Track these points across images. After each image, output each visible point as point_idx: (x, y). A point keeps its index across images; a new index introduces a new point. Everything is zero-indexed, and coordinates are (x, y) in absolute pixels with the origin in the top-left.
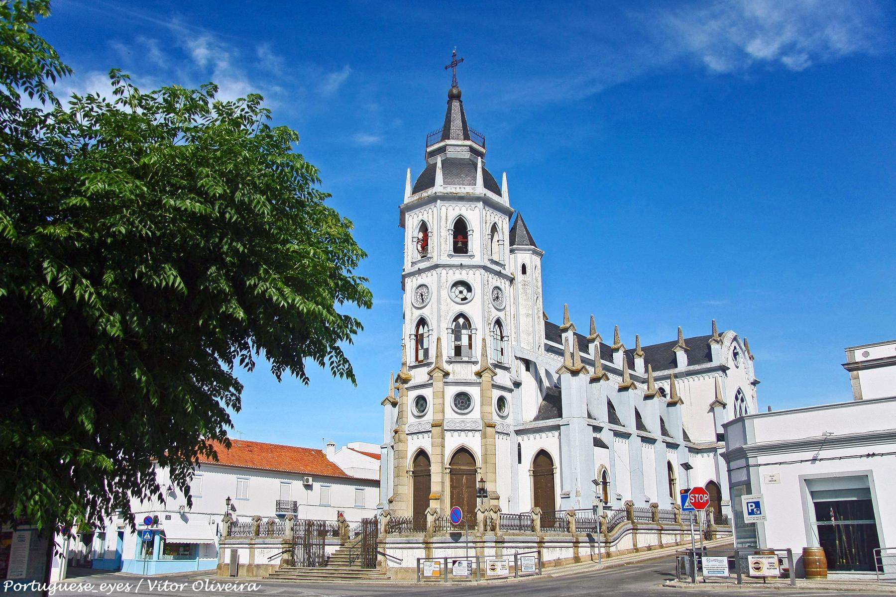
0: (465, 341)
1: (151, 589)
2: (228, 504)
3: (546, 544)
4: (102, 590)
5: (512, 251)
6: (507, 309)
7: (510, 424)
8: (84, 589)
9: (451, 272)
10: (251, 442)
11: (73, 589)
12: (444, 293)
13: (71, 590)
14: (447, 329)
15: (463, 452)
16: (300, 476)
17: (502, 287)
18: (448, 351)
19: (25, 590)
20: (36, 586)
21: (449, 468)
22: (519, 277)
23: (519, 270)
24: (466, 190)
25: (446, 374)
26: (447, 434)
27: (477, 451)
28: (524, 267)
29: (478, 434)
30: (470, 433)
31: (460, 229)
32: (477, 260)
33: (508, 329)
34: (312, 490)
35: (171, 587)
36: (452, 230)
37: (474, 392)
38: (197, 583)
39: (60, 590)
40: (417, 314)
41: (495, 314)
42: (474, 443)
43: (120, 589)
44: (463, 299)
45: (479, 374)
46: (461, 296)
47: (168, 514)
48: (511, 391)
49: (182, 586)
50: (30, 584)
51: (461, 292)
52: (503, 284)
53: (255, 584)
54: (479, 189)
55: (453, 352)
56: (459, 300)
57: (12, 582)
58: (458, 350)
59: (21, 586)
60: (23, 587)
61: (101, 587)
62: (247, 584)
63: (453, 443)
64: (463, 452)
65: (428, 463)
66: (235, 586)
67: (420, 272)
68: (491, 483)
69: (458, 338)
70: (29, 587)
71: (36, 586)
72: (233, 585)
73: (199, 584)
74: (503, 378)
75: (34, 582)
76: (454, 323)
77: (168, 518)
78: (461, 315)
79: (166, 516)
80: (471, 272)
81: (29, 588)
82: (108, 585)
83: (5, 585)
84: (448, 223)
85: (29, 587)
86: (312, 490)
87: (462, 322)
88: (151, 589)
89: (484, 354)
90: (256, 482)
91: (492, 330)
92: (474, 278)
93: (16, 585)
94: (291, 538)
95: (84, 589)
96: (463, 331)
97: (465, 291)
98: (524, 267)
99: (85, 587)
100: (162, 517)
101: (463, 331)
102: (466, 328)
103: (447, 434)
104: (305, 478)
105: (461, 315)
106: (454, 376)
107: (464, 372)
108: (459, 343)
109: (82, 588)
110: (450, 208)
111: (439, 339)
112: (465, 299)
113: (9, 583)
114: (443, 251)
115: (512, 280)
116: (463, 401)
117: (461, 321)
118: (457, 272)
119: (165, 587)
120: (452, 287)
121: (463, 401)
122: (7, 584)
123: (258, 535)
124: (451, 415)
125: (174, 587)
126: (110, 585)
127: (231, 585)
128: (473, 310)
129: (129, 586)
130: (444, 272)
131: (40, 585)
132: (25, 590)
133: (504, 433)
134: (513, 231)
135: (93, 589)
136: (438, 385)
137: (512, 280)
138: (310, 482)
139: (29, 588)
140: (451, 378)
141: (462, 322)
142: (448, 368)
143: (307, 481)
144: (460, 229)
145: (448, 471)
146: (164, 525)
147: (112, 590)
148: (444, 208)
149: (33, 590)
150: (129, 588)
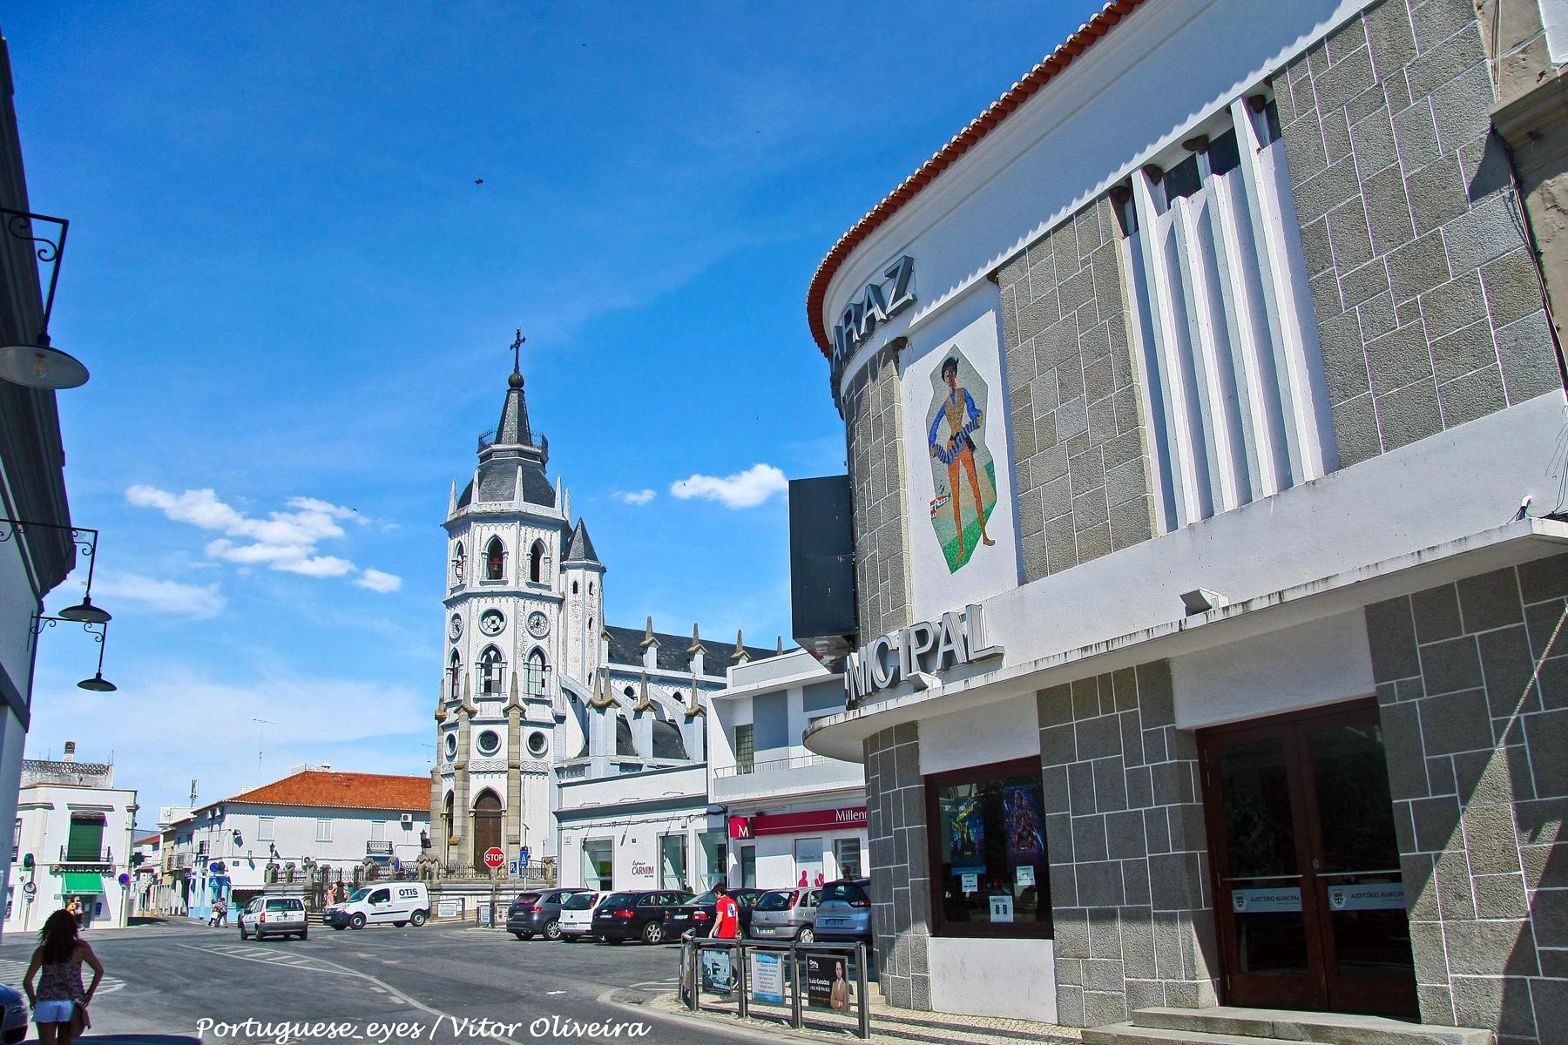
0: (495, 676)
1: (457, 1034)
2: (272, 851)
3: (503, 892)
4: (370, 1035)
5: (563, 569)
6: (553, 634)
7: (550, 760)
8: (338, 1032)
9: (482, 600)
10: (351, 774)
11: (318, 1033)
12: (475, 622)
13: (316, 1035)
14: (476, 664)
15: (488, 794)
16: (394, 814)
17: (547, 613)
18: (476, 688)
19: (234, 1034)
20: (254, 1028)
21: (473, 812)
22: (570, 596)
23: (569, 589)
24: (503, 506)
25: (472, 713)
26: (472, 777)
27: (502, 791)
28: (575, 585)
29: (505, 775)
30: (496, 776)
31: (496, 551)
32: (511, 587)
33: (551, 660)
34: (411, 829)
35: (493, 1028)
36: (485, 554)
37: (502, 731)
38: (538, 1022)
39: (297, 1034)
40: (488, 641)
41: (532, 643)
42: (499, 784)
43: (402, 1033)
44: (495, 630)
45: (506, 711)
46: (494, 626)
47: (237, 860)
48: (551, 726)
49: (511, 1029)
50: (243, 1025)
51: (493, 622)
52: (550, 610)
53: (640, 1025)
54: (518, 504)
55: (483, 687)
56: (490, 631)
57: (212, 1021)
58: (488, 686)
59: (227, 1027)
60: (231, 1030)
61: (369, 1030)
62: (626, 1024)
63: (477, 785)
64: (488, 794)
65: (498, 803)
66: (606, 1027)
67: (492, 595)
68: (514, 827)
69: (489, 673)
70: (242, 1030)
71: (254, 1028)
72: (602, 1026)
73: (543, 1024)
74: (535, 712)
75: (250, 1022)
76: (485, 656)
77: (236, 864)
78: (492, 647)
79: (234, 862)
80: (504, 600)
81: (242, 1031)
82: (380, 1027)
83: (199, 1026)
84: (482, 546)
85: (242, 1030)
86: (411, 829)
87: (491, 657)
88: (457, 1034)
89: (514, 690)
90: (339, 825)
91: (526, 661)
92: (506, 606)
93: (218, 1026)
94: (310, 884)
95: (338, 1032)
96: (495, 665)
97: (498, 621)
98: (575, 585)
99: (341, 1029)
100: (228, 863)
101: (495, 665)
102: (498, 662)
103: (472, 777)
104: (403, 815)
105: (492, 647)
106: (481, 714)
107: (493, 710)
108: (489, 677)
109: (334, 1032)
110: (485, 528)
111: (514, 674)
112: (498, 628)
113: (207, 1024)
114: (475, 578)
115: (561, 602)
116: (489, 740)
117: (492, 653)
118: (489, 600)
119: (481, 1030)
120: (483, 619)
121: (489, 740)
122: (203, 1024)
123: (291, 881)
124: (476, 756)
125: (498, 1030)
126: (385, 1027)
127: (598, 1025)
128: (504, 642)
129: (419, 1028)
130: (475, 601)
131: (260, 1026)
132: (234, 1034)
133: (537, 773)
134: (566, 548)
135: (355, 1034)
136: (463, 725)
137: (561, 602)
138: (410, 820)
139: (242, 1031)
140: (478, 717)
141: (491, 657)
142: (476, 706)
143: (406, 818)
144: (496, 551)
145: (472, 814)
146: (231, 872)
147: (388, 1034)
148: (478, 529)
149: (248, 1034)
150: (418, 1032)
